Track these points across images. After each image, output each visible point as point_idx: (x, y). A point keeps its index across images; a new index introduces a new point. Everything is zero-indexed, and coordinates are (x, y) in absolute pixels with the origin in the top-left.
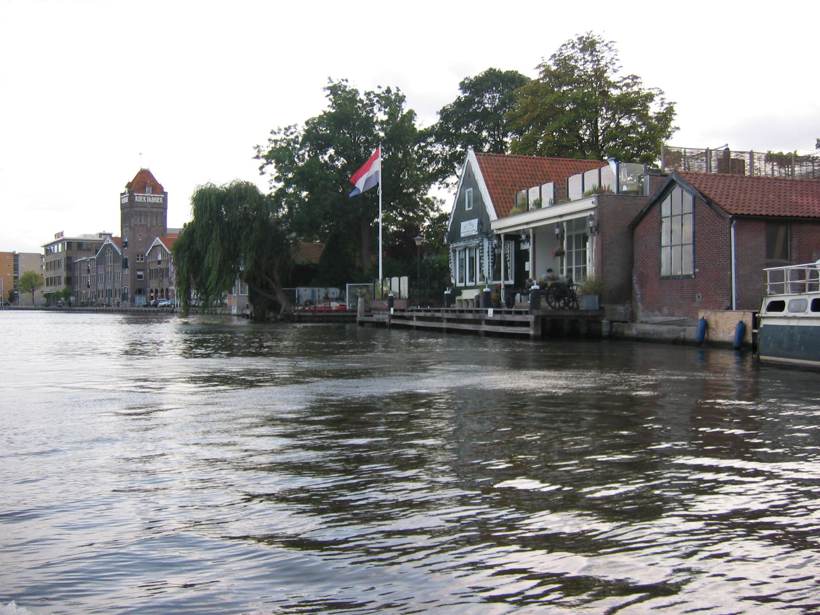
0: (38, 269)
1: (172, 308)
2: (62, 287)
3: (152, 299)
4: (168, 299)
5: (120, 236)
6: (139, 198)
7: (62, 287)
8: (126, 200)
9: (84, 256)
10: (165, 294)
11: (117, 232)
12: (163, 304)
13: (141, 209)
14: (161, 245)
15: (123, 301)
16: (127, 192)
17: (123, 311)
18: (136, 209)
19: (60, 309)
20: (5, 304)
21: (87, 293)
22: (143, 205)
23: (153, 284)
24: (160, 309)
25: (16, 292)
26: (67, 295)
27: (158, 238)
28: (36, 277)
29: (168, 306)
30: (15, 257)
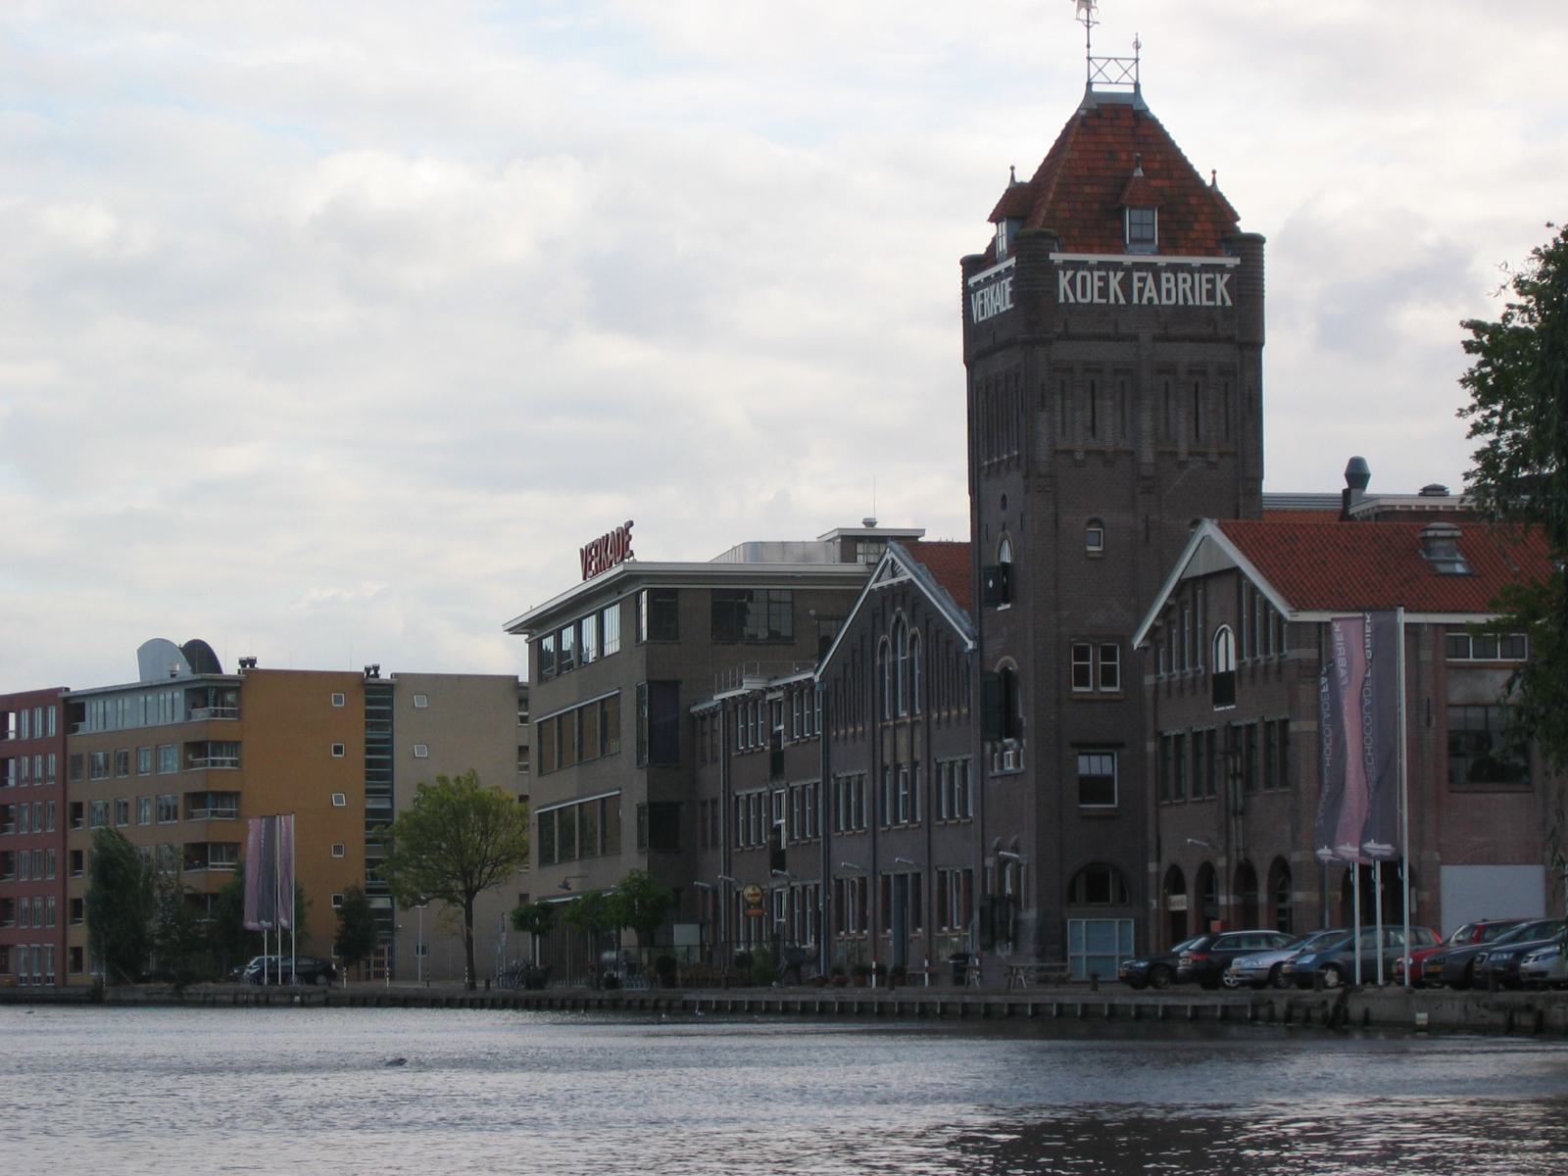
0: (493, 766)
1: (1332, 995)
2: (627, 862)
3: (1179, 936)
4: (1286, 923)
5: (962, 534)
6: (1083, 279)
7: (627, 862)
8: (998, 300)
9: (751, 671)
10: (1263, 897)
11: (946, 515)
12: (1267, 961)
13: (1099, 352)
14: (1236, 571)
15: (988, 947)
16: (1003, 245)
17: (989, 1012)
18: (1063, 351)
19: (603, 997)
20: (308, 977)
21: (768, 899)
22: (1106, 323)
23: (1187, 835)
24: (1244, 998)
25: (380, 903)
26: (651, 910)
27: (1209, 529)
28: (485, 809)
29: (1304, 978)
30: (375, 696)
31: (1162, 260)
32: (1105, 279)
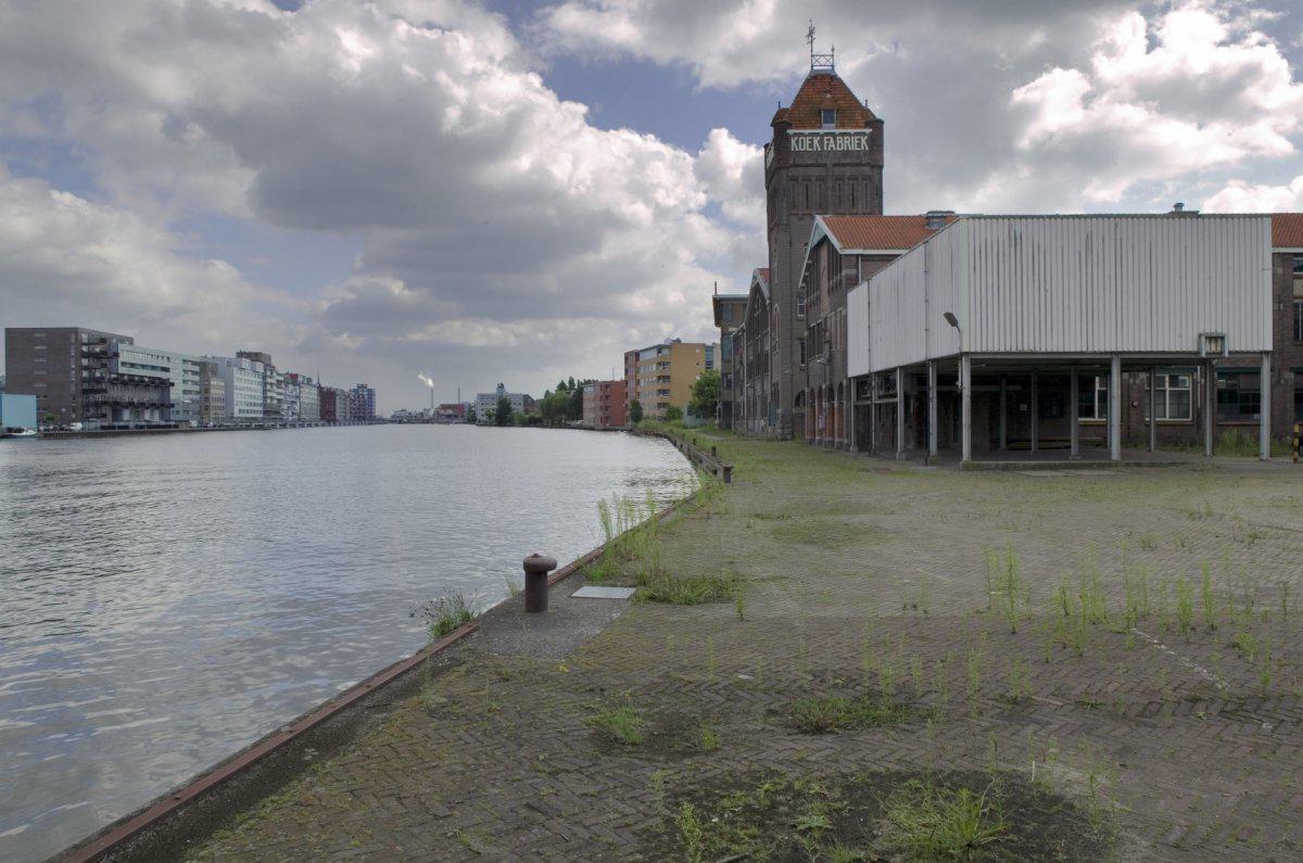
31: (837, 131)
32: (811, 140)
